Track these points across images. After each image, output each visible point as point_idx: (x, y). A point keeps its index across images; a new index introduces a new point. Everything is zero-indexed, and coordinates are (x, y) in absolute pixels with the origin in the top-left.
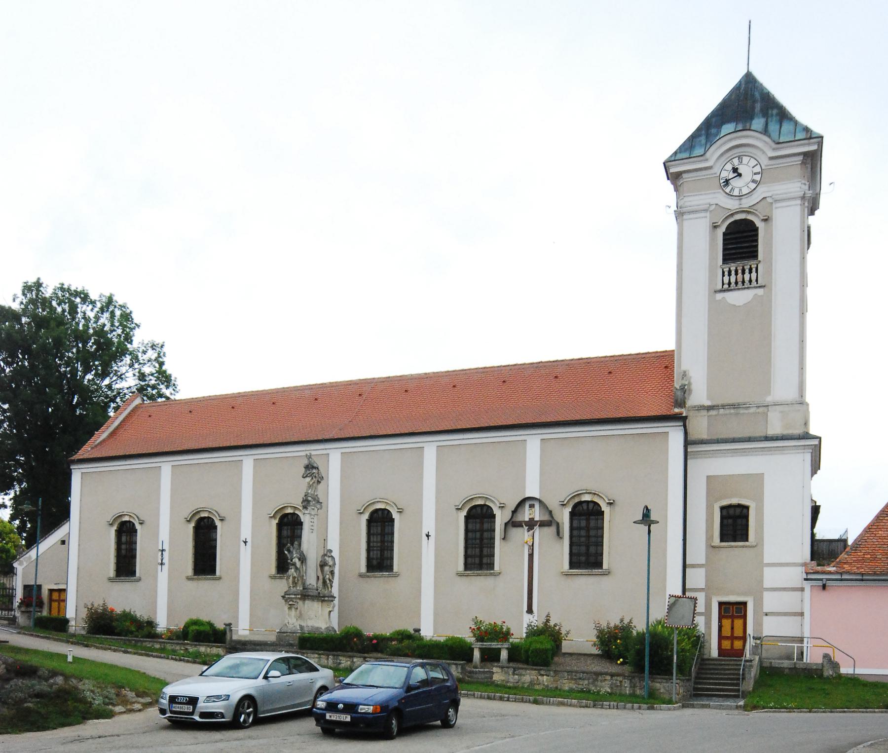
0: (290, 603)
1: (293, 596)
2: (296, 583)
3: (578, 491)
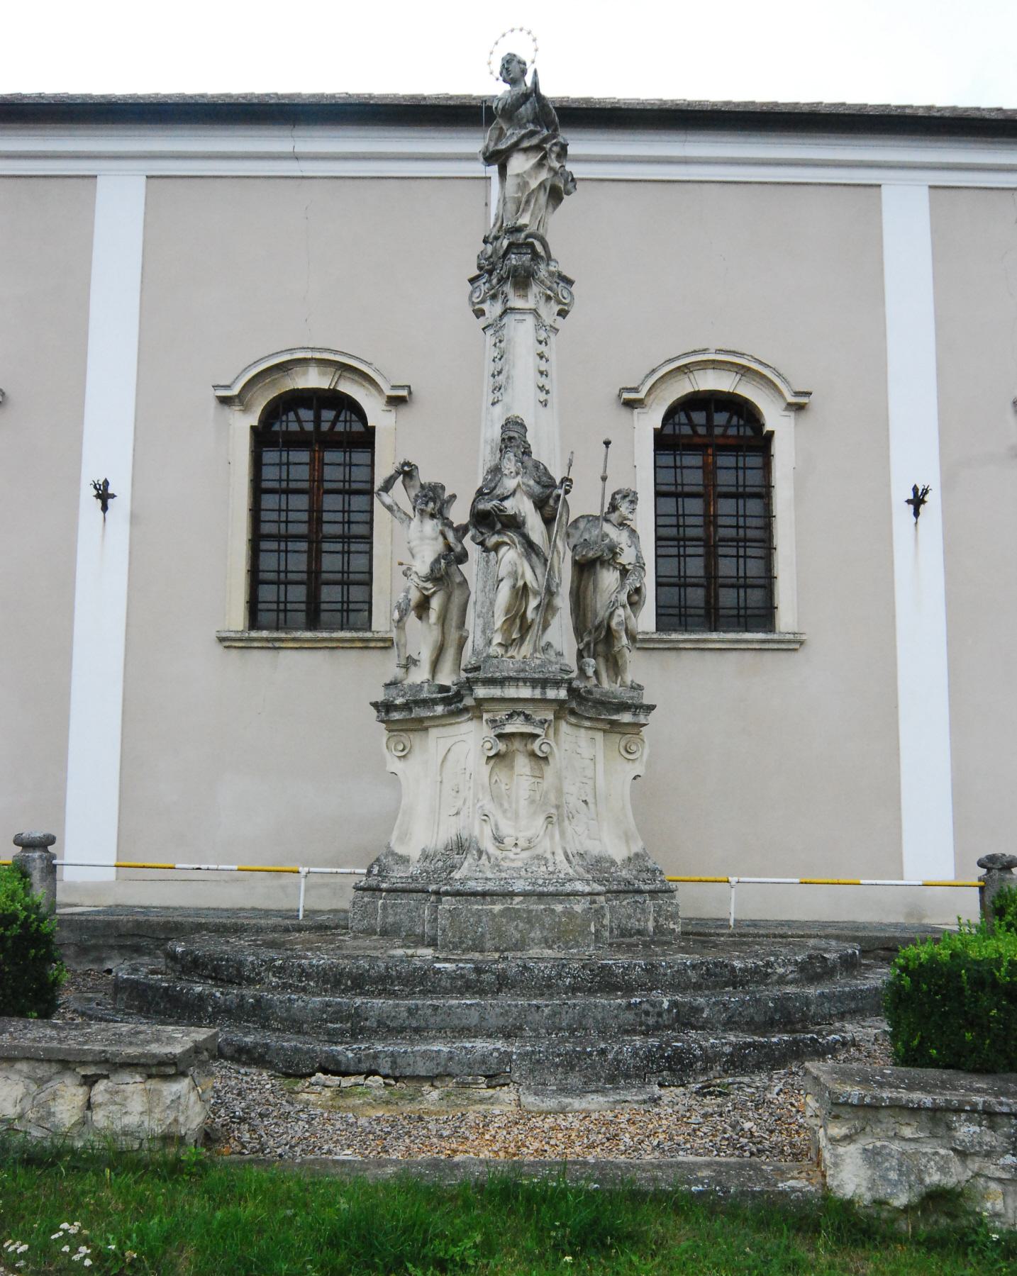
0: (509, 729)
1: (525, 692)
2: (525, 628)
3: (767, 366)
